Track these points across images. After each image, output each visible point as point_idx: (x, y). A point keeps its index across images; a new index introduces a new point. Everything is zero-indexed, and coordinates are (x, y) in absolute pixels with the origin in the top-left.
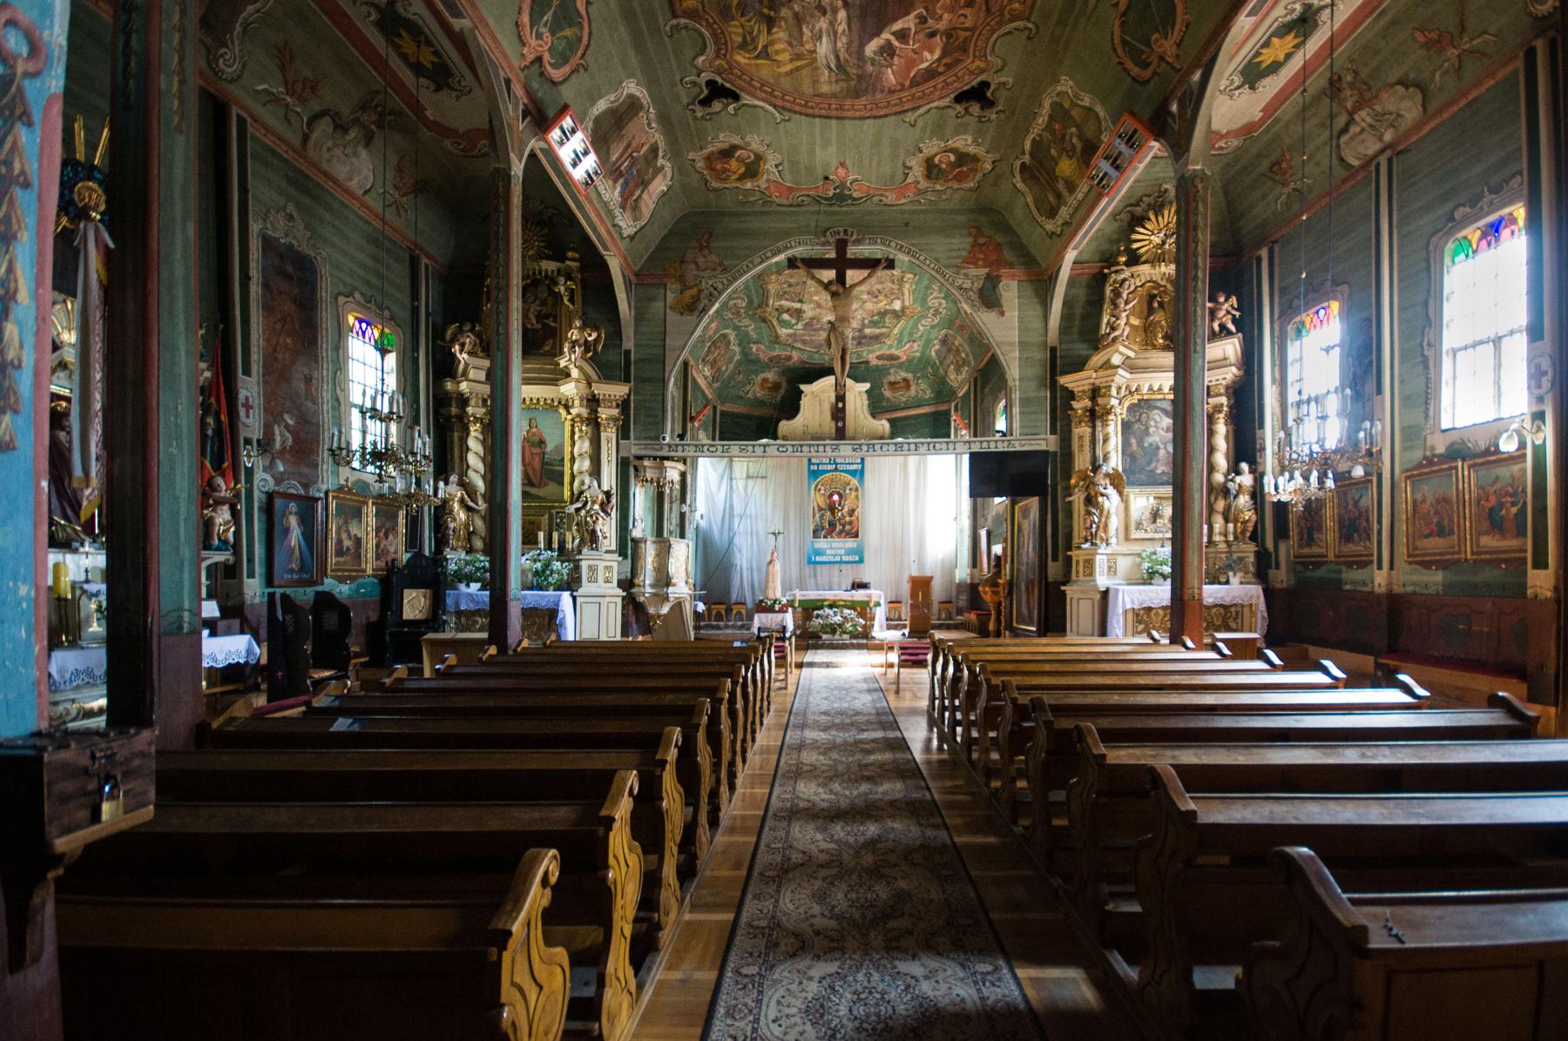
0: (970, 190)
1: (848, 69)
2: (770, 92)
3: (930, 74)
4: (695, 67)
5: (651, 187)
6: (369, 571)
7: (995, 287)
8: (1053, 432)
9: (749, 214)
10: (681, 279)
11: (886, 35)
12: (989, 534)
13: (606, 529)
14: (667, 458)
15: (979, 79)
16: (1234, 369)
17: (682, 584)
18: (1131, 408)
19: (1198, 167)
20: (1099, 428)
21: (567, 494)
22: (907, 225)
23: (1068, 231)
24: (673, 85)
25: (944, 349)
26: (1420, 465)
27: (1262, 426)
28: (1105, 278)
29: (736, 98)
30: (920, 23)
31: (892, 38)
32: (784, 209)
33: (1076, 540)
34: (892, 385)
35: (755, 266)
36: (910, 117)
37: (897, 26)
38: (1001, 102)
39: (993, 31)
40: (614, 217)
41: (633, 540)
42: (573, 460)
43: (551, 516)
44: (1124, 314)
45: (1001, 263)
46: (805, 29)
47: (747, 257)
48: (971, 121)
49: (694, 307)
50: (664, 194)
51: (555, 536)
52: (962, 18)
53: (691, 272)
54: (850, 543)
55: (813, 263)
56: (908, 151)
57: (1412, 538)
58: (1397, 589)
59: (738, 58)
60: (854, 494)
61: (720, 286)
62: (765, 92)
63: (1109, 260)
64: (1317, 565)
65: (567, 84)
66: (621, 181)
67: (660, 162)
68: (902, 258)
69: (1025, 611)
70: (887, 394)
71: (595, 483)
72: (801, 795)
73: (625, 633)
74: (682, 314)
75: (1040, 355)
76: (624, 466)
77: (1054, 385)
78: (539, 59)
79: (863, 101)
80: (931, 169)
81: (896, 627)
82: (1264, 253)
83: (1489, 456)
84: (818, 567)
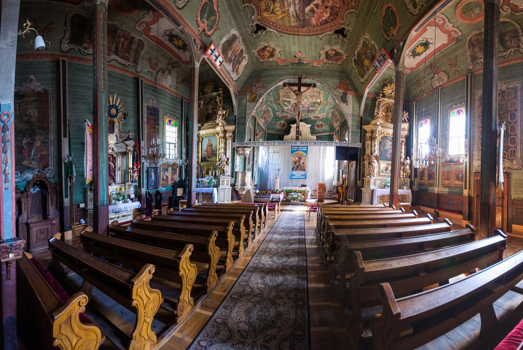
0: (339, 65)
2: (275, 26)
3: (326, 22)
4: (252, 20)
5: (242, 64)
6: (170, 184)
7: (346, 96)
8: (360, 142)
9: (271, 69)
10: (251, 92)
11: (312, 5)
12: (342, 171)
13: (227, 169)
14: (246, 147)
15: (342, 27)
16: (407, 132)
17: (249, 185)
18: (382, 138)
19: (401, 70)
20: (373, 143)
21: (218, 159)
22: (320, 74)
24: (246, 28)
25: (332, 116)
26: (444, 163)
27: (412, 148)
28: (376, 99)
29: (265, 29)
31: (314, 7)
32: (282, 67)
33: (365, 175)
34: (318, 125)
35: (273, 86)
36: (320, 36)
38: (348, 37)
39: (346, 10)
40: (230, 75)
41: (235, 172)
42: (219, 149)
43: (213, 166)
44: (381, 110)
45: (348, 89)
46: (285, 2)
47: (271, 83)
48: (340, 41)
49: (254, 100)
50: (246, 65)
51: (214, 171)
52: (336, 3)
53: (254, 89)
54: (303, 173)
55: (290, 85)
56: (320, 49)
57: (443, 180)
58: (439, 193)
60: (304, 158)
61: (262, 93)
62: (274, 26)
63: (377, 94)
64: (423, 185)
65: (213, 35)
66: (232, 63)
67: (244, 55)
68: (318, 84)
69: (351, 195)
70: (316, 128)
71: (225, 156)
72: (261, 261)
73: (232, 200)
74: (251, 102)
75: (358, 119)
76: (233, 150)
77: (361, 128)
78: (204, 30)
79: (305, 29)
80: (327, 55)
81: (315, 198)
82: (414, 103)
83: (457, 162)
84: (293, 180)
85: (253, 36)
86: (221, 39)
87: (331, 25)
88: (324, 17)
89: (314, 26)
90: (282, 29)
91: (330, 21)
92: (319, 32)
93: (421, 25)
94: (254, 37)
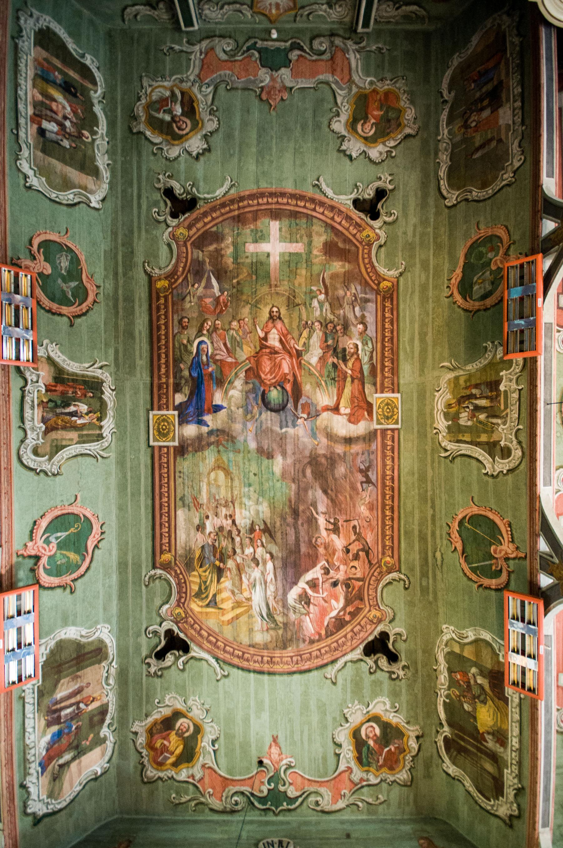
1: (275, 616)
3: (340, 623)
5: (85, 759)
9: (175, 822)
11: (302, 584)
22: (348, 836)
23: (525, 801)
24: (138, 635)
29: (186, 648)
30: (325, 574)
31: (307, 587)
36: (330, 671)
37: (309, 576)
39: (378, 581)
40: (26, 774)
48: (382, 676)
52: (353, 569)
59: (194, 606)
62: (210, 642)
65: (50, 592)
66: (55, 729)
67: (105, 731)
78: (37, 558)
79: (290, 651)
85: (149, 665)
86: (66, 622)
87: (352, 630)
88: (332, 610)
89: (312, 642)
90: (228, 653)
91: (347, 618)
92: (327, 658)
93: (545, 459)
94: (153, 670)
